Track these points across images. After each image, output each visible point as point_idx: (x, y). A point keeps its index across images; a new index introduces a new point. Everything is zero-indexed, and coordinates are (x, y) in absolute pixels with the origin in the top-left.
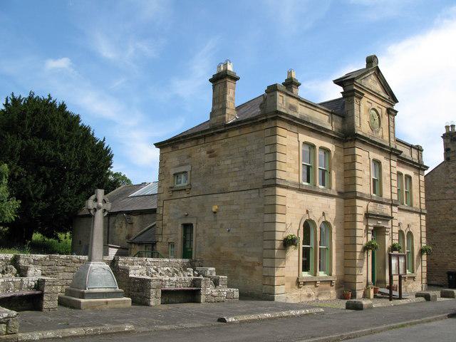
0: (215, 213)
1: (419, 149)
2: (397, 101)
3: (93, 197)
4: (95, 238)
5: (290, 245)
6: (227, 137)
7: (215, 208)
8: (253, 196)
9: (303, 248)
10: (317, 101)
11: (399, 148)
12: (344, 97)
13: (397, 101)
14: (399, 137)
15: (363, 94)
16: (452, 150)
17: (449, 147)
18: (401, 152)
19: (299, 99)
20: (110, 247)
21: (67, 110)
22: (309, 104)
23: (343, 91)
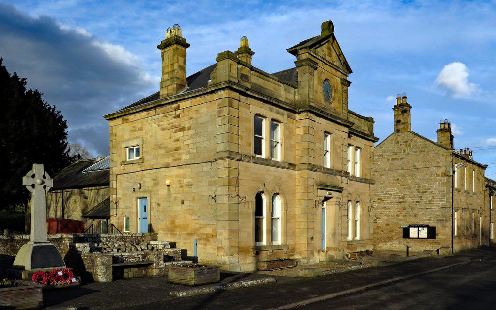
0: (168, 186)
1: (371, 121)
2: (351, 72)
3: (30, 173)
4: (263, 144)
5: (41, 103)
6: (178, 108)
7: (167, 182)
8: (205, 169)
9: (136, 156)
10: (270, 71)
11: (352, 119)
12: (298, 67)
13: (351, 72)
14: (350, 108)
15: (317, 64)
16: (402, 121)
17: (399, 119)
18: (353, 124)
19: (252, 69)
20: (18, 241)
21: (27, 88)
22: (263, 74)
23: (296, 60)
